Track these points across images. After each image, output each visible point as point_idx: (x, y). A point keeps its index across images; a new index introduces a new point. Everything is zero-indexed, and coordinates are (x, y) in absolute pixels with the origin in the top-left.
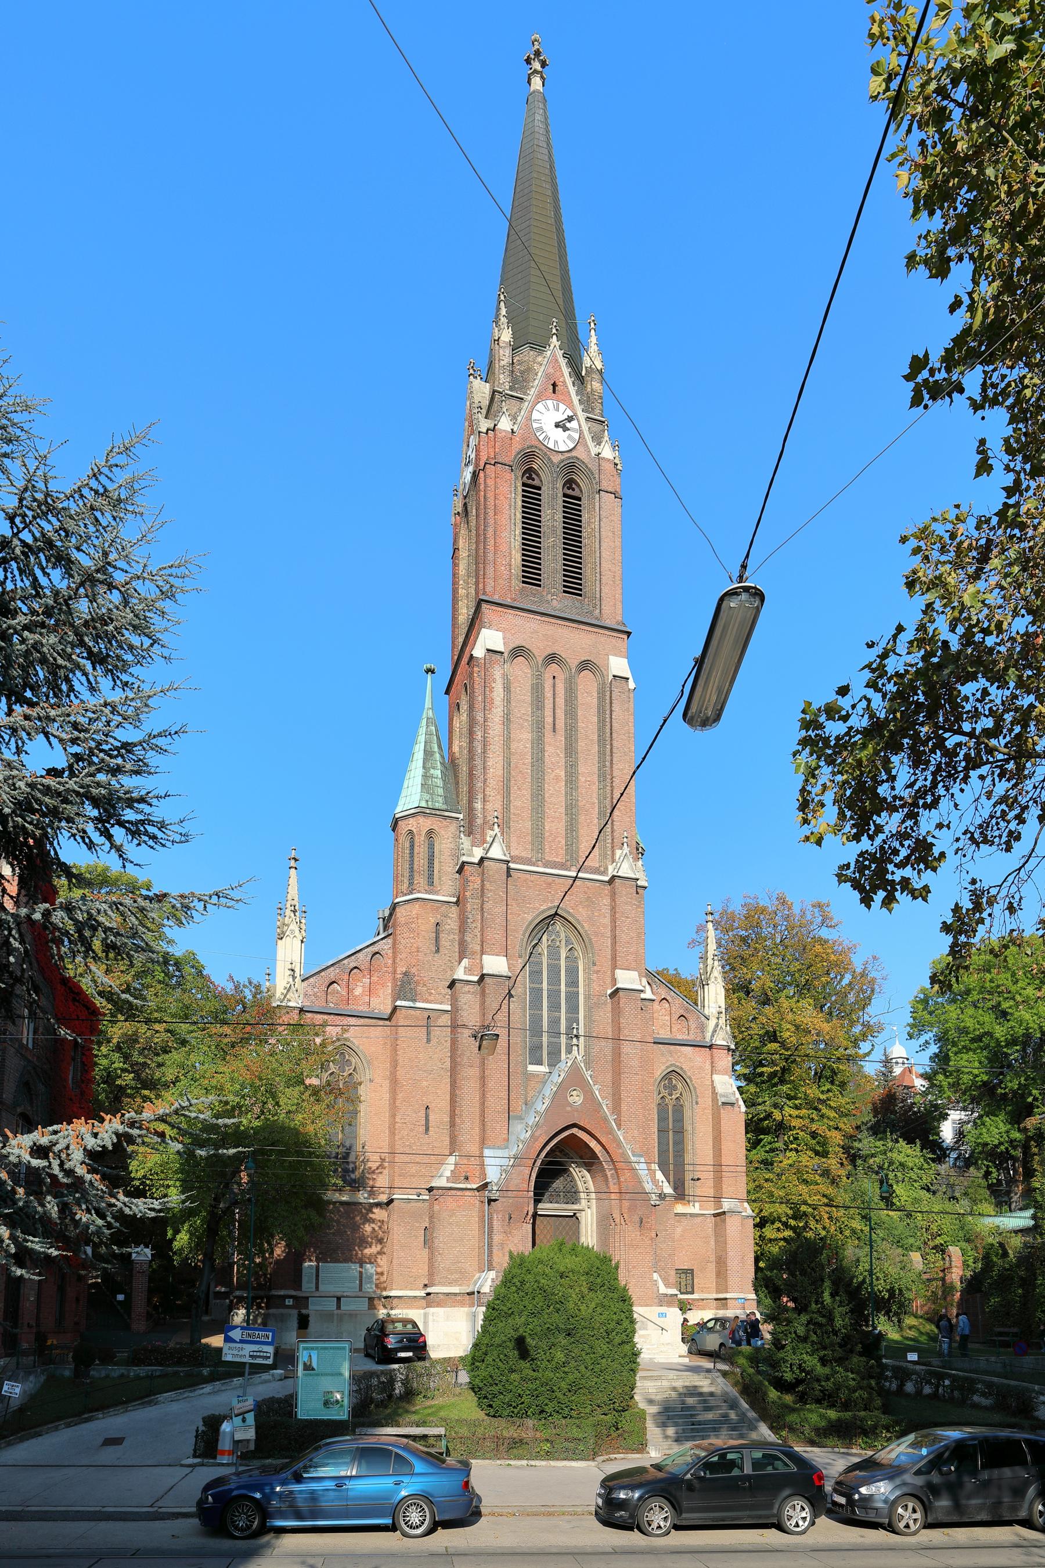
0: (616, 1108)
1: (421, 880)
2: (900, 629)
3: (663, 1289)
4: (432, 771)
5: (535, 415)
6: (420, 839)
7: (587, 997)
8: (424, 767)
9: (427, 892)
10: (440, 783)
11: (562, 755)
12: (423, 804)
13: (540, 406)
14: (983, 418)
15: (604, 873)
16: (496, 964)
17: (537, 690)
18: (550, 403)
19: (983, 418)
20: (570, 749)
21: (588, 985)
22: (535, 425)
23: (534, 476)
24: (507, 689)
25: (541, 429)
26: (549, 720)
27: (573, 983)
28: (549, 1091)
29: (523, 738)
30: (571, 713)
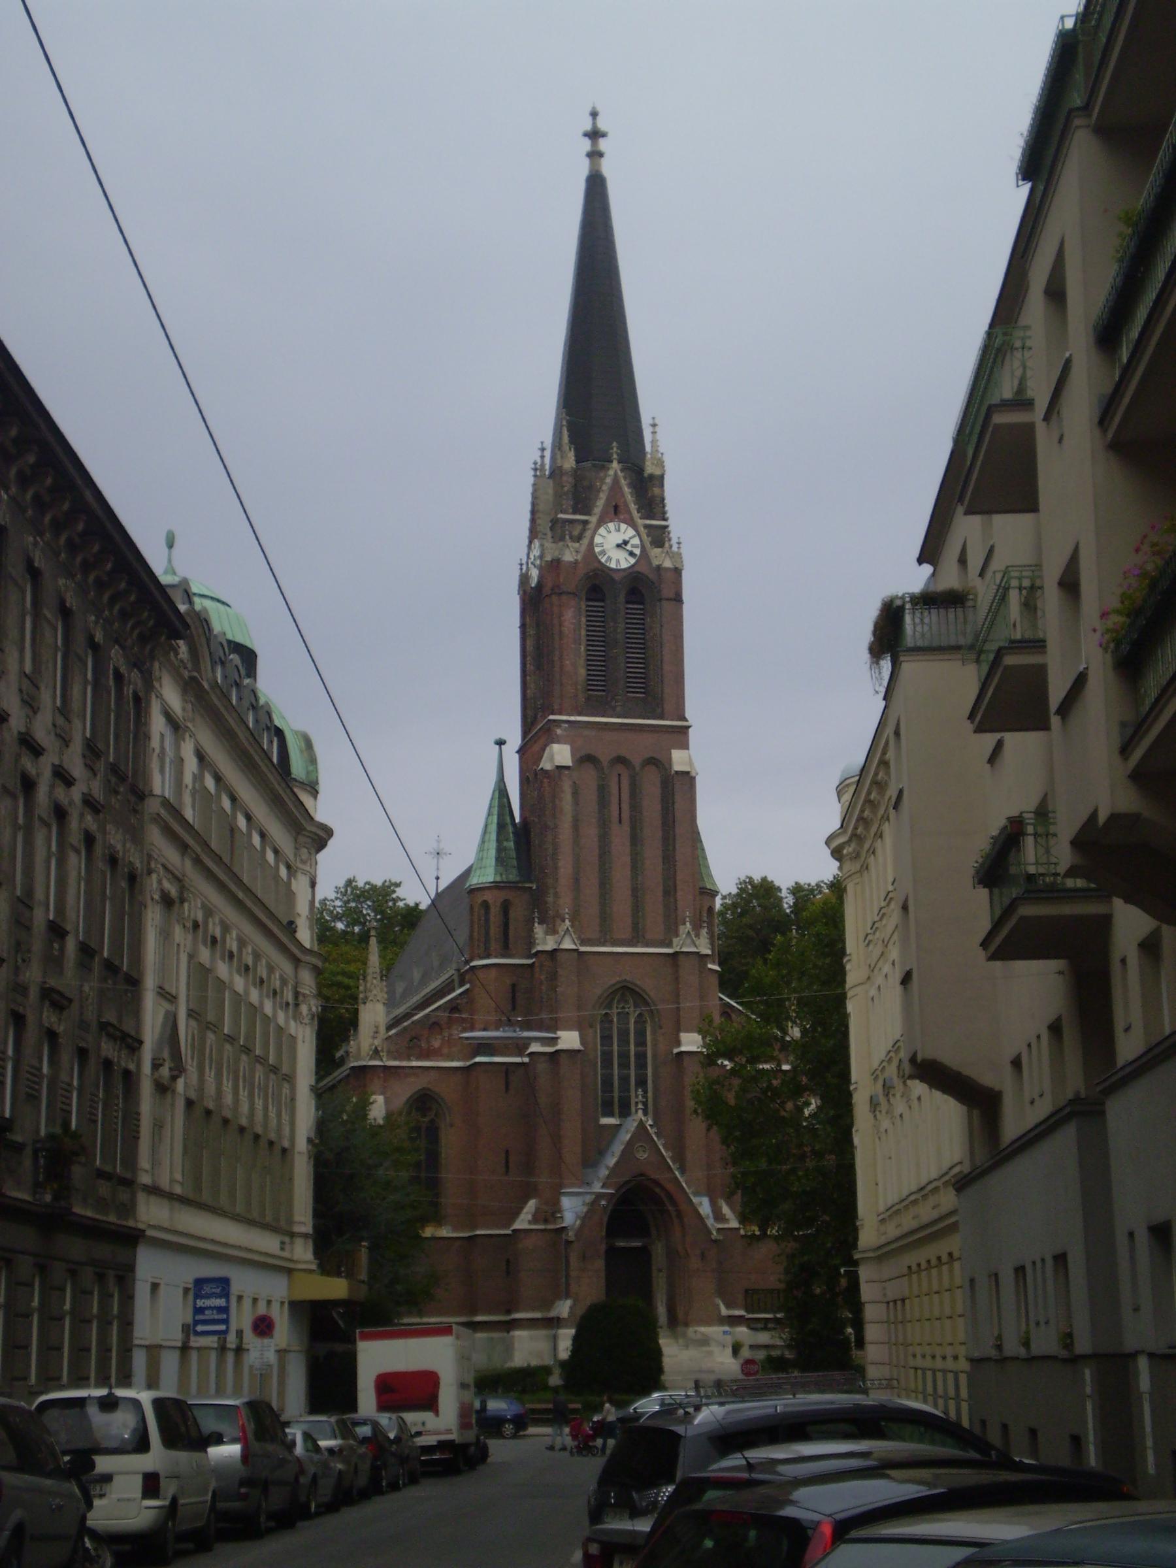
0: (680, 1158)
1: (494, 946)
2: (543, 450)
3: (724, 1311)
4: (505, 844)
5: (598, 540)
6: (495, 911)
7: (655, 1056)
8: (498, 840)
9: (503, 956)
10: (513, 854)
11: (628, 844)
12: (498, 879)
13: (602, 531)
14: (1095, 630)
15: (670, 945)
16: (569, 1039)
17: (602, 790)
18: (611, 526)
19: (1095, 630)
20: (635, 839)
21: (655, 1045)
22: (597, 550)
23: (717, 1019)
24: (575, 794)
25: (603, 552)
26: (615, 813)
27: (641, 1042)
28: (617, 1148)
29: (591, 832)
30: (635, 807)
